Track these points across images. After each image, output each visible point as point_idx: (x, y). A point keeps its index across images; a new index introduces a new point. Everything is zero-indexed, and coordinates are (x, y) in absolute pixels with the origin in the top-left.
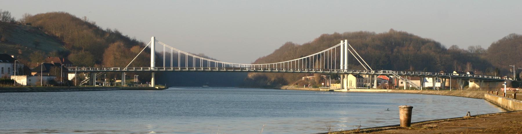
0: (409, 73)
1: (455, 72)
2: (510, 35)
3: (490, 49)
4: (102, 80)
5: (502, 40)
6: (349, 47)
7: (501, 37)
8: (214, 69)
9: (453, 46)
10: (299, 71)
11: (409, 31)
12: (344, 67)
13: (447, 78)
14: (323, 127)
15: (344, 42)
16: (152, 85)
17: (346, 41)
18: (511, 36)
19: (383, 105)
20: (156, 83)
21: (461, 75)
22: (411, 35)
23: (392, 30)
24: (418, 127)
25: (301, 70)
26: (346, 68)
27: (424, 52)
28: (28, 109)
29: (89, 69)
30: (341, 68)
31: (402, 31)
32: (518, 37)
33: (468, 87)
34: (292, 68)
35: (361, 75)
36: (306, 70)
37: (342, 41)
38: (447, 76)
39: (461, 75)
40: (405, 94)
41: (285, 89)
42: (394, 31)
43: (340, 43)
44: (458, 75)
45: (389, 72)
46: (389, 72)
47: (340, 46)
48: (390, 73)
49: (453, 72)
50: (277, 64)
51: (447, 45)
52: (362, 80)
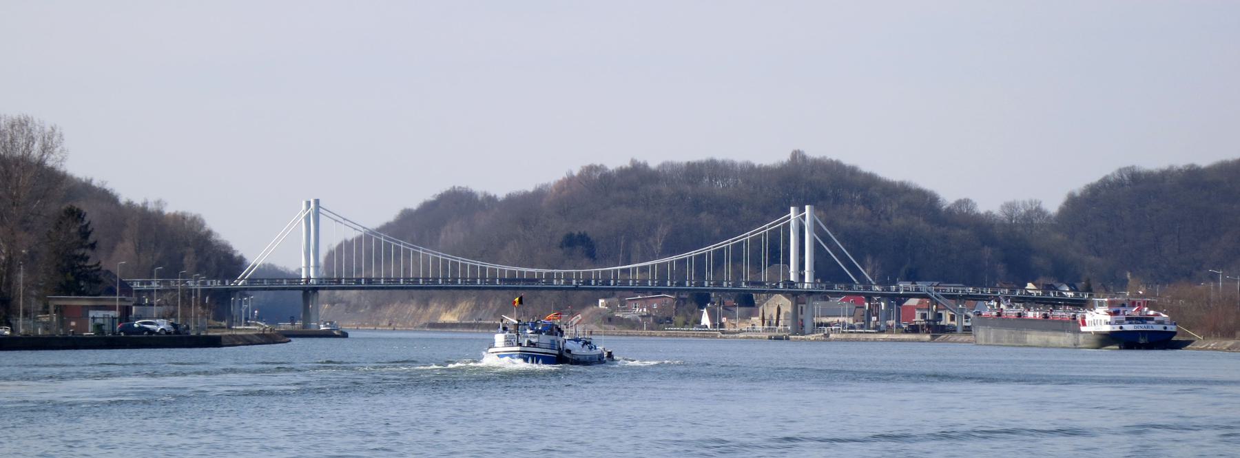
1: (1030, 286)
2: (1120, 171)
3: (1063, 211)
5: (1097, 185)
6: (817, 229)
7: (1094, 177)
11: (848, 160)
13: (602, 298)
18: (1125, 176)
21: (1081, 295)
22: (853, 171)
23: (633, 161)
24: (121, 368)
27: (898, 222)
28: (256, 419)
29: (223, 283)
31: (828, 157)
35: (1064, 293)
38: (1037, 292)
39: (1081, 295)
40: (1035, 349)
41: (102, 316)
42: (804, 157)
44: (1072, 294)
49: (1027, 285)
51: (948, 196)
52: (802, 307)
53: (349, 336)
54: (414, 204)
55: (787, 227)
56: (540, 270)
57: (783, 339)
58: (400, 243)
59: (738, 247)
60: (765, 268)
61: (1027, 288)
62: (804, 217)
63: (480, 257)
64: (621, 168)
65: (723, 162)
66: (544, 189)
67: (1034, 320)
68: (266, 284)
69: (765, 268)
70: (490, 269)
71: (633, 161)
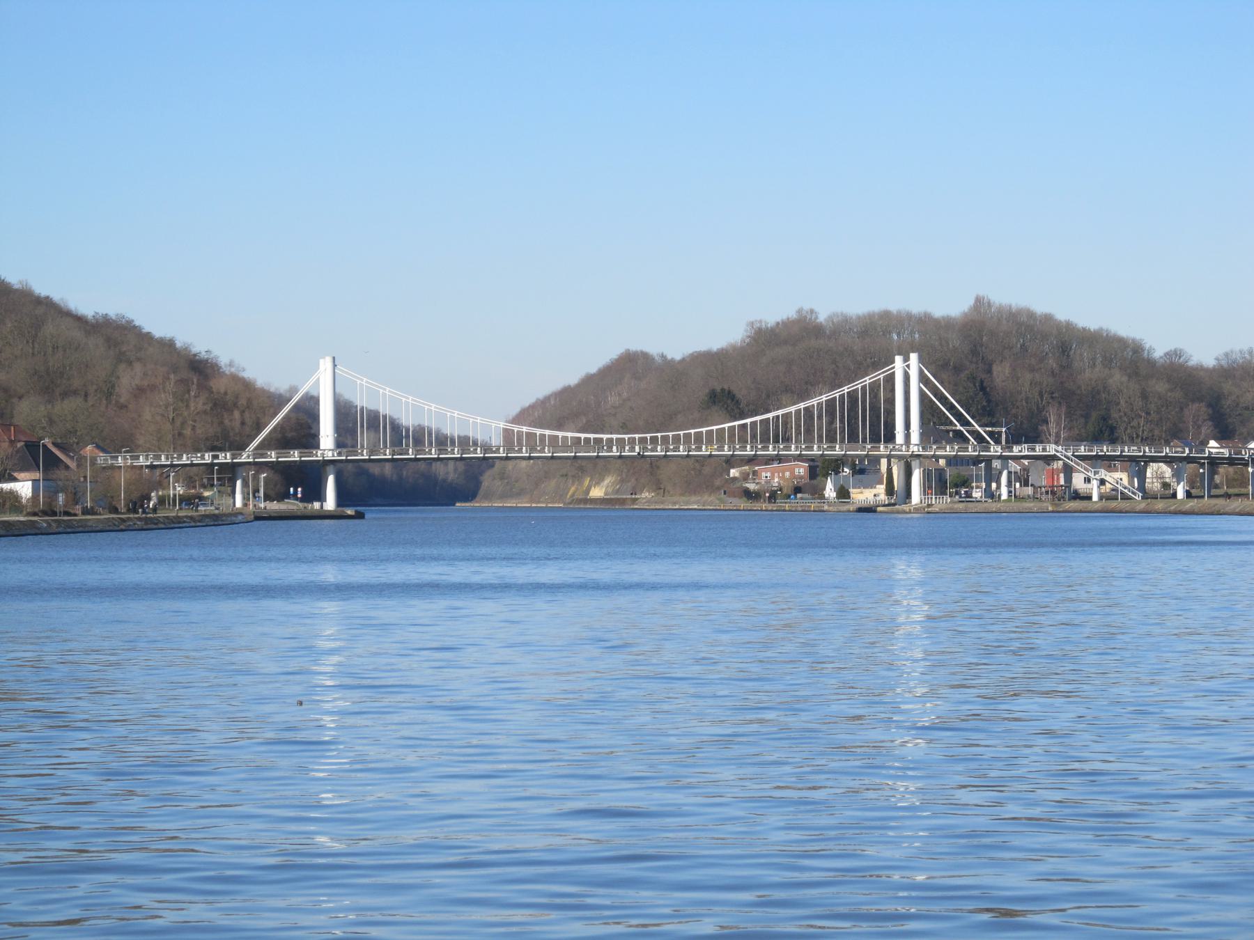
0: (1105, 450)
4: (192, 482)
6: (923, 379)
8: (446, 452)
9: (1227, 355)
10: (617, 452)
11: (1040, 306)
12: (907, 437)
14: (380, 779)
15: (906, 359)
16: (330, 503)
17: (914, 357)
19: (1227, 703)
20: (342, 499)
25: (645, 449)
26: (915, 437)
29: (203, 457)
30: (900, 438)
31: (702, 350)
32: (688, 360)
33: (910, 502)
34: (526, 446)
36: (546, 450)
37: (899, 360)
43: (893, 362)
45: (1044, 450)
46: (1044, 450)
47: (894, 373)
48: (1051, 453)
49: (1208, 443)
50: (651, 437)
51: (1158, 346)
53: (366, 516)
54: (593, 370)
55: (890, 379)
56: (609, 436)
57: (1157, 498)
58: (454, 413)
59: (831, 403)
60: (362, 433)
61: (1209, 446)
62: (908, 366)
63: (560, 428)
64: (9, 283)
65: (899, 312)
66: (1224, 363)
67: (991, 486)
68: (141, 461)
69: (362, 433)
70: (563, 437)
71: (799, 311)
